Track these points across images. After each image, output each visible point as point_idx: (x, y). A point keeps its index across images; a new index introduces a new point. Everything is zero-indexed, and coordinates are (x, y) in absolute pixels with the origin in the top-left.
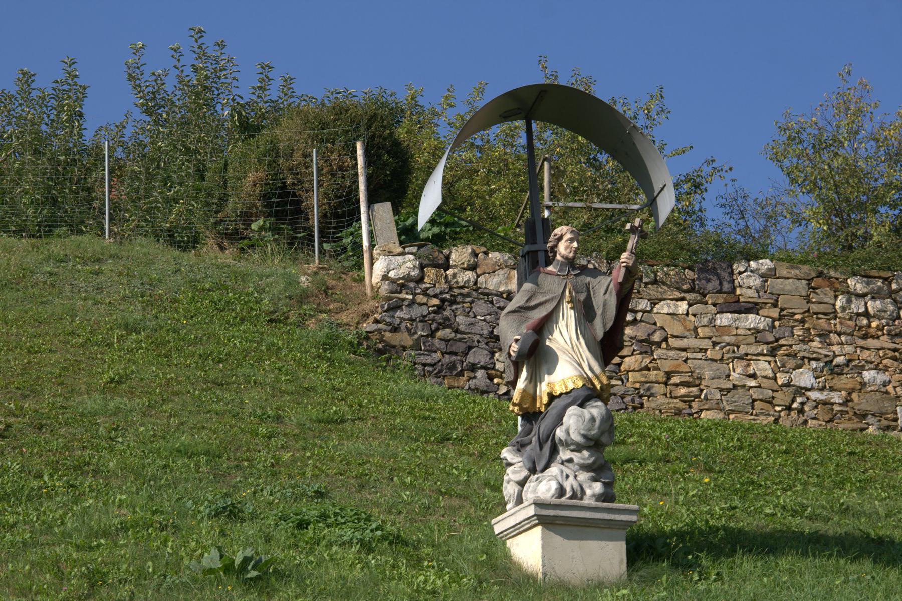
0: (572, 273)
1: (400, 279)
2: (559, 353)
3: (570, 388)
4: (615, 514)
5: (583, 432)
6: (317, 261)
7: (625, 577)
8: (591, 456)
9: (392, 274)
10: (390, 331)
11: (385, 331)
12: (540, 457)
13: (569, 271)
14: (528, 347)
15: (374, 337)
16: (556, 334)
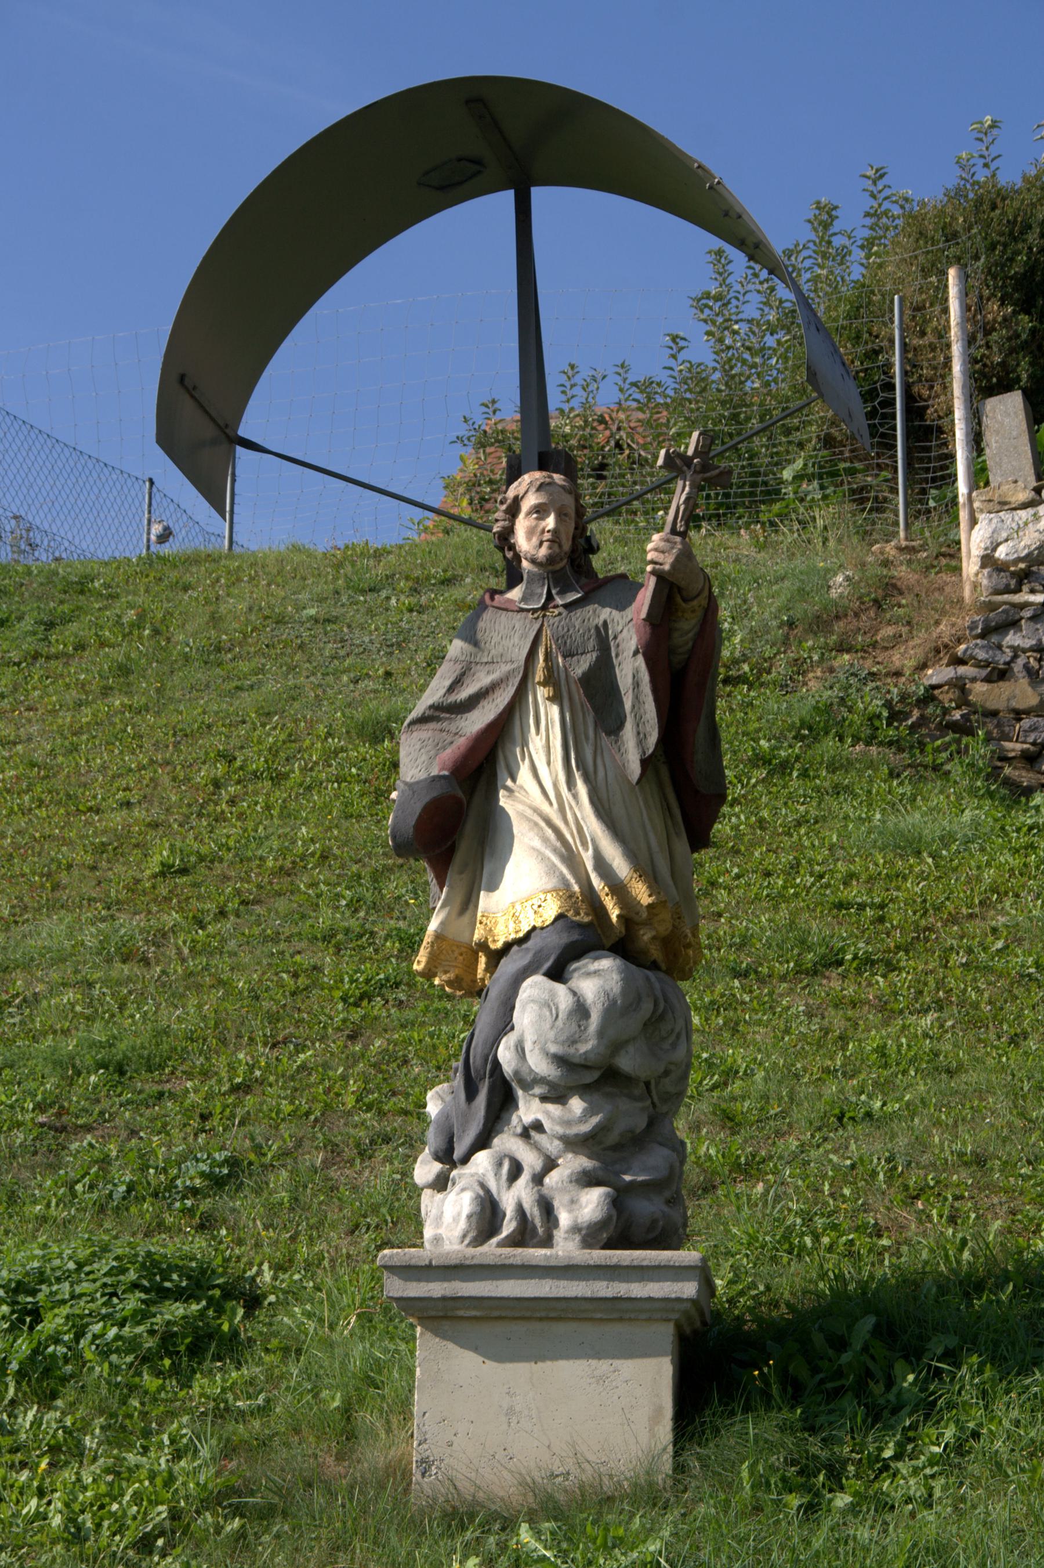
0: (559, 601)
1: (1020, 560)
2: (519, 828)
3: (525, 928)
4: (628, 1281)
5: (553, 1049)
6: (902, 534)
7: (667, 1464)
8: (588, 1113)
9: (1001, 553)
10: (988, 680)
11: (974, 680)
12: (466, 1120)
13: (550, 597)
14: (412, 821)
15: (947, 697)
16: (524, 774)
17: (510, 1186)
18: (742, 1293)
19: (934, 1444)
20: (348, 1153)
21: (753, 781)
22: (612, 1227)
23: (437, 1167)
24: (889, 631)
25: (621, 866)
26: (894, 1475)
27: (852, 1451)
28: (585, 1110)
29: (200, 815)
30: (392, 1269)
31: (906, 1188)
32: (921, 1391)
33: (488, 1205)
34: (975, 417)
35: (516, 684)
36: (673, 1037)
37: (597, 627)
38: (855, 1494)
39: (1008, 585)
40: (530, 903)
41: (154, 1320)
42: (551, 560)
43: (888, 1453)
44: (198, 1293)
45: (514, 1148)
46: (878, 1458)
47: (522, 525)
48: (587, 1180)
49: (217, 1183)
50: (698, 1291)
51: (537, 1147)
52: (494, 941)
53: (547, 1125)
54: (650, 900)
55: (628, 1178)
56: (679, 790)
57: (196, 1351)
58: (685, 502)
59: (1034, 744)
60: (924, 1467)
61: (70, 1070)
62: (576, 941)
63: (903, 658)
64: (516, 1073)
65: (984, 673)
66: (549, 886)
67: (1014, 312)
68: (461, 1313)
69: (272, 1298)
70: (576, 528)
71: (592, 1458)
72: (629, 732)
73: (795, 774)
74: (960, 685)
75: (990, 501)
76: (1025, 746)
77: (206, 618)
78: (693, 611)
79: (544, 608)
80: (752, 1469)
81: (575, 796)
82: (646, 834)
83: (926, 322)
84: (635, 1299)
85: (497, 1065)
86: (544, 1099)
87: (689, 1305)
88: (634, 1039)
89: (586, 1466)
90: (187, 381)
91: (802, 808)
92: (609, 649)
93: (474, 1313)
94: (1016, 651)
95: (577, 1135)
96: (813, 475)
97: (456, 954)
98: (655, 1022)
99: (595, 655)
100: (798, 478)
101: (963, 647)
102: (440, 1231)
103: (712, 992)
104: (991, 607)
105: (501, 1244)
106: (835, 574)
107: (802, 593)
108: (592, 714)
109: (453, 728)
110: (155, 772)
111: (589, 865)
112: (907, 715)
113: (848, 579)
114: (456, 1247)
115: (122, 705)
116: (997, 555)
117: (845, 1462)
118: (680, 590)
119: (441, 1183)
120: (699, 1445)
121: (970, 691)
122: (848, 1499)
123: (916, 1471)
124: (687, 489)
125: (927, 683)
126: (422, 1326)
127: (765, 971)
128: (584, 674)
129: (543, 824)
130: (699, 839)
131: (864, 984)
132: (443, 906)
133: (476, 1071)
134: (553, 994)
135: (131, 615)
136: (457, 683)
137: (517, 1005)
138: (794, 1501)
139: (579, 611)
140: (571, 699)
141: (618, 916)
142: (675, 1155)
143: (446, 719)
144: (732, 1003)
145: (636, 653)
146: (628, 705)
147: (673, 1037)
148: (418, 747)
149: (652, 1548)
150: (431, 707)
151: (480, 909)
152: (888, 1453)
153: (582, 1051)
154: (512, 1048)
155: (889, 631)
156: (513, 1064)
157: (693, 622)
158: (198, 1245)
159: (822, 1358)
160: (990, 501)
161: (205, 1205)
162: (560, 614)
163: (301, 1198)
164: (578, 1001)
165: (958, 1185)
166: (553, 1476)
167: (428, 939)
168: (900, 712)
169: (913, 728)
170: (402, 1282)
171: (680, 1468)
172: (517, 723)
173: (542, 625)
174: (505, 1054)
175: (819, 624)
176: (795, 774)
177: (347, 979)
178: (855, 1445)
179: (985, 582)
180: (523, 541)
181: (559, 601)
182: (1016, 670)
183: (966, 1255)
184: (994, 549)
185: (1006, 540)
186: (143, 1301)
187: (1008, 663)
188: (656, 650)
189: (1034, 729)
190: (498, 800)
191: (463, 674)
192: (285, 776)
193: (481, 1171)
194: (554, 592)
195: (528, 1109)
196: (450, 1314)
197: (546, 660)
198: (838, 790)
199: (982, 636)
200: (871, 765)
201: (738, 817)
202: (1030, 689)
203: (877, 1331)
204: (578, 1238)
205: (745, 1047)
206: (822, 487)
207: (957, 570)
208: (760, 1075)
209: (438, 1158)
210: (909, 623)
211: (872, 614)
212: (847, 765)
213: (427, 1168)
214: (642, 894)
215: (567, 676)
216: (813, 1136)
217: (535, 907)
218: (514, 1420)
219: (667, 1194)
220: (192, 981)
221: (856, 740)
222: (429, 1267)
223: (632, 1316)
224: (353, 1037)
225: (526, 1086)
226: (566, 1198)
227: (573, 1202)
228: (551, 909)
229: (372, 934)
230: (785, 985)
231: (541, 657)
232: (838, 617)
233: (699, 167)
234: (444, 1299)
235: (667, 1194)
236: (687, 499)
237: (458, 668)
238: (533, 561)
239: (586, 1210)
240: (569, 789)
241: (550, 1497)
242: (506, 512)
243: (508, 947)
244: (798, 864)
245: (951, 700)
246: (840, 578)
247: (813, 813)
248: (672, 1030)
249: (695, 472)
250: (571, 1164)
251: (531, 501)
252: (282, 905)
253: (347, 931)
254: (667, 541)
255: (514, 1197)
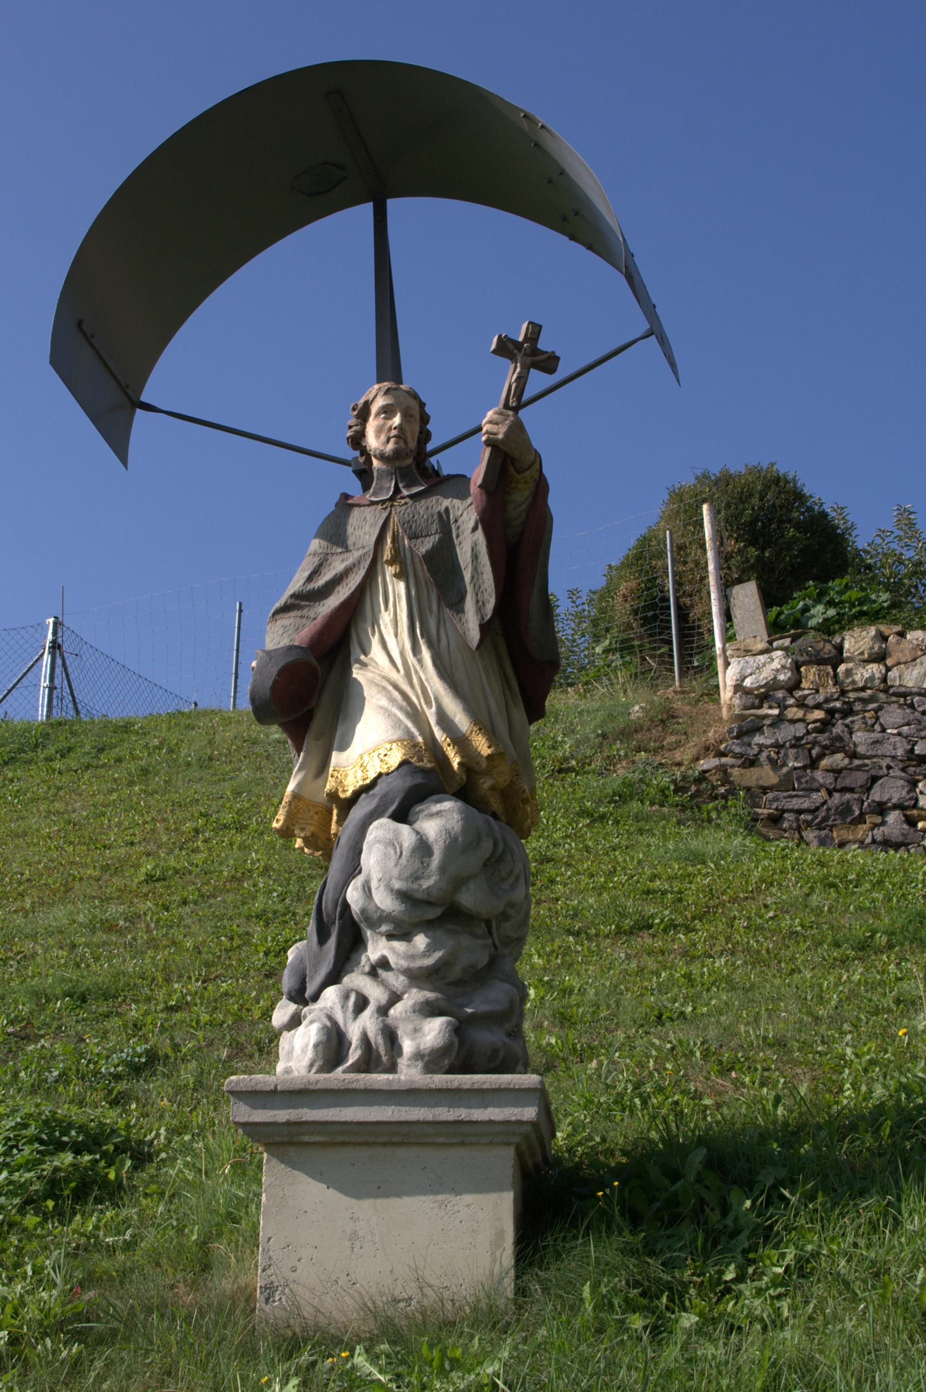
0: (405, 493)
2: (369, 692)
3: (372, 775)
5: (397, 885)
6: (677, 684)
8: (430, 949)
9: (748, 683)
10: (742, 766)
11: (733, 766)
12: (317, 961)
13: (397, 490)
14: (269, 683)
15: (714, 779)
17: (355, 1018)
18: (580, 1144)
19: (775, 1266)
20: (249, 1049)
21: (581, 825)
22: (454, 1054)
23: (292, 1007)
24: (673, 739)
25: (461, 720)
26: (737, 1298)
27: (693, 1274)
28: (428, 945)
29: (181, 849)
30: (238, 1094)
31: (720, 1063)
32: (758, 1216)
33: (334, 1035)
34: (725, 598)
35: (367, 566)
36: (512, 879)
37: (439, 513)
38: (700, 1315)
39: (753, 703)
40: (377, 753)
41: (44, 1166)
42: (397, 455)
43: (729, 1276)
44: (93, 1148)
45: (362, 984)
46: (719, 1281)
47: (372, 425)
48: (429, 1010)
49: (136, 1069)
50: (538, 1114)
51: (384, 983)
52: (344, 791)
53: (392, 960)
54: (489, 751)
55: (469, 1010)
56: (517, 656)
57: (80, 1195)
58: (516, 381)
59: (776, 809)
60: (768, 1288)
61: (42, 998)
62: (420, 784)
63: (684, 755)
64: (363, 911)
65: (739, 762)
66: (395, 737)
67: (745, 546)
68: (306, 1138)
69: (163, 1155)
70: (421, 432)
71: (435, 1282)
72: (470, 605)
73: (610, 822)
74: (723, 769)
75: (738, 649)
76: (771, 811)
77: (206, 742)
78: (526, 483)
79: (392, 499)
80: (595, 1287)
81: (420, 661)
82: (486, 699)
83: (687, 555)
84: (476, 1122)
85: (346, 906)
86: (390, 937)
87: (528, 1128)
88: (475, 876)
89: (429, 1292)
90: (84, 327)
91: (616, 840)
92: (450, 532)
93: (318, 1138)
94: (761, 747)
95: (420, 968)
96: (616, 649)
97: (312, 813)
98: (493, 863)
99: (437, 537)
100: (606, 651)
101: (723, 746)
102: (290, 1064)
103: (552, 945)
104: (741, 718)
105: (344, 1072)
106: (633, 706)
107: (611, 717)
108: (435, 591)
109: (312, 614)
110: (155, 825)
111: (432, 721)
112: (688, 789)
113: (641, 708)
114: (303, 1072)
115: (141, 790)
116: (745, 684)
117: (685, 1285)
118: (513, 461)
119: (295, 1022)
120: (540, 1268)
121: (731, 775)
122: (695, 1319)
123: (759, 1292)
124: (518, 369)
125: (700, 769)
126: (268, 1153)
127: (593, 931)
128: (427, 552)
129: (390, 688)
130: (535, 711)
131: (669, 940)
132: (299, 770)
133: (328, 915)
134: (397, 834)
135: (156, 742)
136: (315, 573)
137: (365, 848)
138: (637, 1322)
139: (423, 502)
140: (416, 577)
141: (459, 764)
142: (515, 990)
143: (307, 606)
144: (567, 951)
145: (475, 529)
146: (467, 576)
147: (512, 879)
148: (280, 632)
149: (490, 1370)
150: (293, 596)
151: (332, 765)
152: (729, 1276)
153: (424, 887)
154: (360, 889)
155: (673, 739)
156: (360, 903)
157: (526, 493)
158: (111, 1117)
159: (658, 1189)
160: (738, 649)
161: (122, 1086)
162: (406, 503)
163: (205, 1081)
164: (421, 838)
165: (765, 1060)
166: (396, 1301)
167: (286, 799)
168: (683, 787)
169: (692, 797)
170: (248, 1108)
171: (521, 1291)
172: (368, 602)
173: (390, 513)
174: (353, 895)
175: (626, 734)
176: (610, 822)
177: (270, 939)
178: (696, 1267)
179: (737, 702)
180: (373, 441)
181: (405, 493)
182: (762, 760)
183: (780, 1111)
184: (743, 681)
185: (751, 674)
186: (39, 1152)
187: (756, 755)
188: (490, 521)
189: (776, 799)
190: (351, 673)
191: (320, 565)
192: (246, 827)
193: (329, 1004)
194: (401, 485)
195: (375, 949)
196: (295, 1139)
197: (393, 542)
198: (641, 831)
199: (737, 737)
200: (664, 818)
201: (570, 844)
202: (772, 772)
203: (709, 1164)
204: (420, 1064)
205: (576, 863)
206: (622, 657)
207: (717, 701)
208: (592, 992)
209: (292, 999)
210: (685, 733)
211: (660, 729)
212: (648, 818)
213: (283, 1011)
214: (482, 746)
215: (412, 557)
216: (637, 1032)
217: (382, 756)
218: (357, 1244)
219: (508, 1026)
220: (153, 944)
221: (652, 804)
222: (274, 1092)
223: (474, 1140)
224: (268, 976)
225: (374, 924)
226: (410, 1027)
227: (416, 1030)
228: (396, 757)
229: (294, 914)
230: (608, 941)
231: (389, 541)
232: (636, 731)
233: (525, 116)
234: (288, 1123)
235: (508, 1026)
236: (518, 378)
237: (316, 560)
238: (382, 457)
239: (428, 1038)
240: (415, 655)
241: (389, 1320)
242: (357, 417)
243: (357, 794)
244: (615, 870)
245: (717, 780)
246: (637, 708)
247: (624, 843)
248: (512, 871)
249: (525, 354)
250: (414, 997)
251: (380, 402)
252: (230, 897)
253: (275, 912)
254: (500, 414)
255: (361, 1027)
